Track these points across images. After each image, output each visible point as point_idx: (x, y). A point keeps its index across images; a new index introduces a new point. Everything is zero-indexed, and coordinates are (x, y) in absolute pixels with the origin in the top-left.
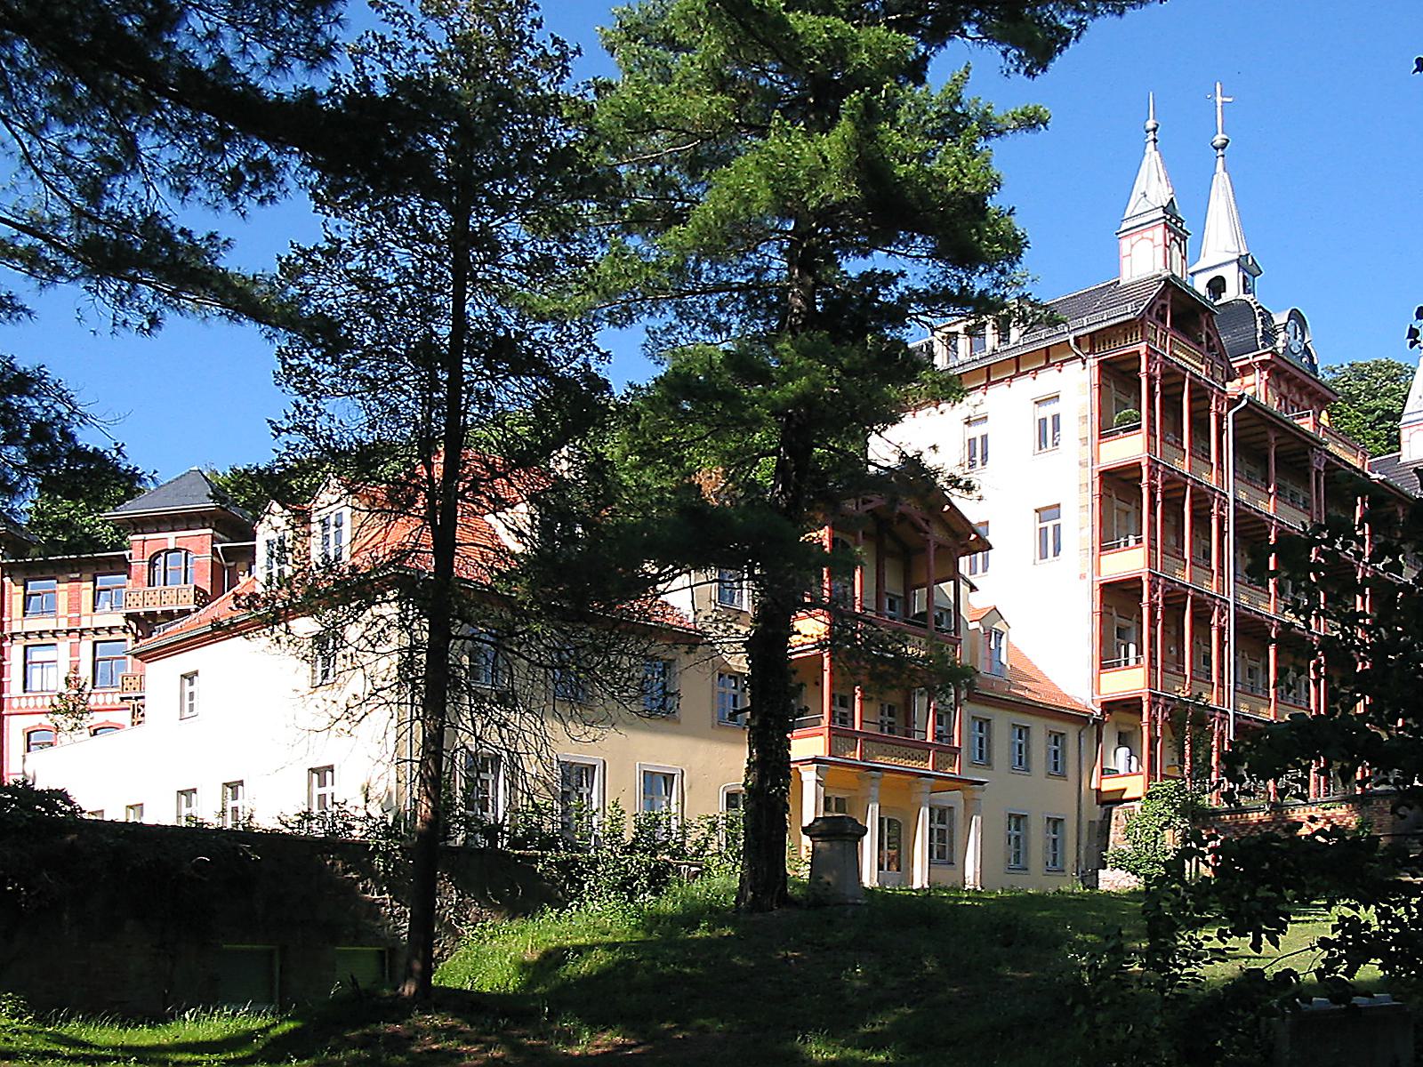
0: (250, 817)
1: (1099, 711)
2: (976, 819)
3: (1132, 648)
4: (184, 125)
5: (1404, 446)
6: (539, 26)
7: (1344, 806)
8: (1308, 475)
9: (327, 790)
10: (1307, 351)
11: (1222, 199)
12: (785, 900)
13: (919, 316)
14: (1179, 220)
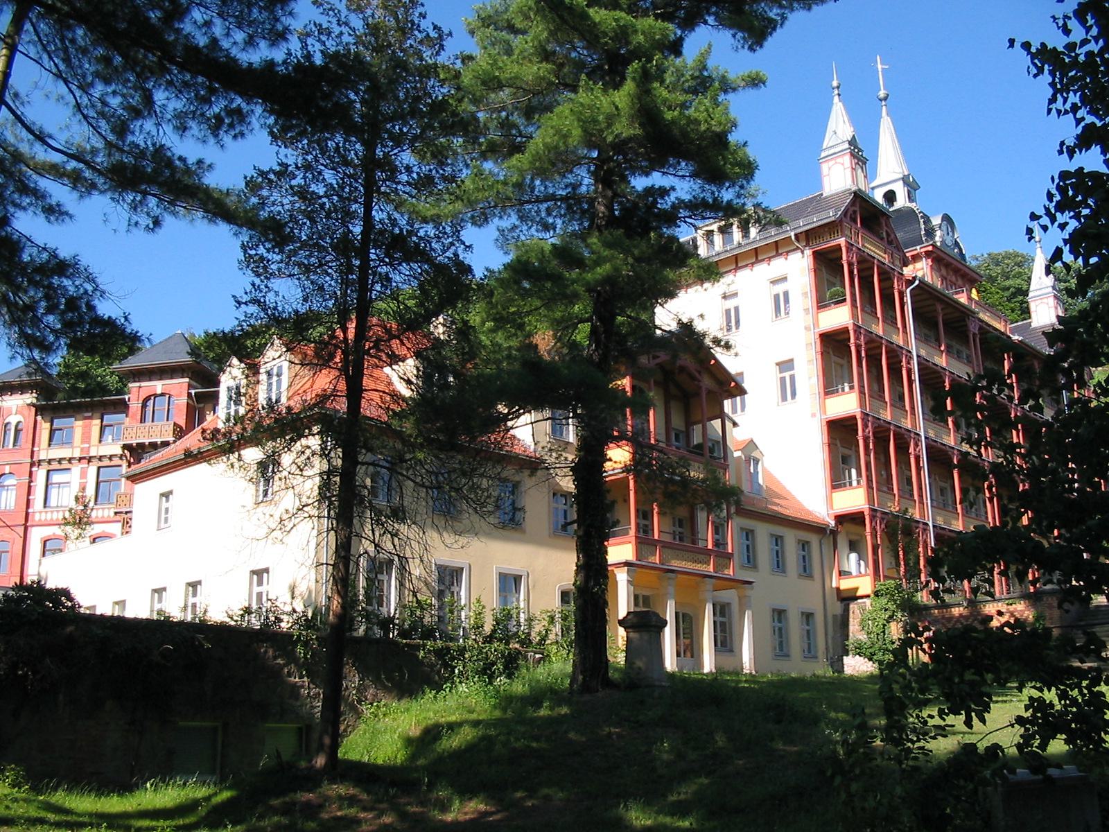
1: (833, 523)
2: (748, 615)
3: (854, 472)
5: (1033, 315)
6: (424, 18)
8: (968, 337)
10: (957, 244)
12: (609, 684)
14: (860, 150)
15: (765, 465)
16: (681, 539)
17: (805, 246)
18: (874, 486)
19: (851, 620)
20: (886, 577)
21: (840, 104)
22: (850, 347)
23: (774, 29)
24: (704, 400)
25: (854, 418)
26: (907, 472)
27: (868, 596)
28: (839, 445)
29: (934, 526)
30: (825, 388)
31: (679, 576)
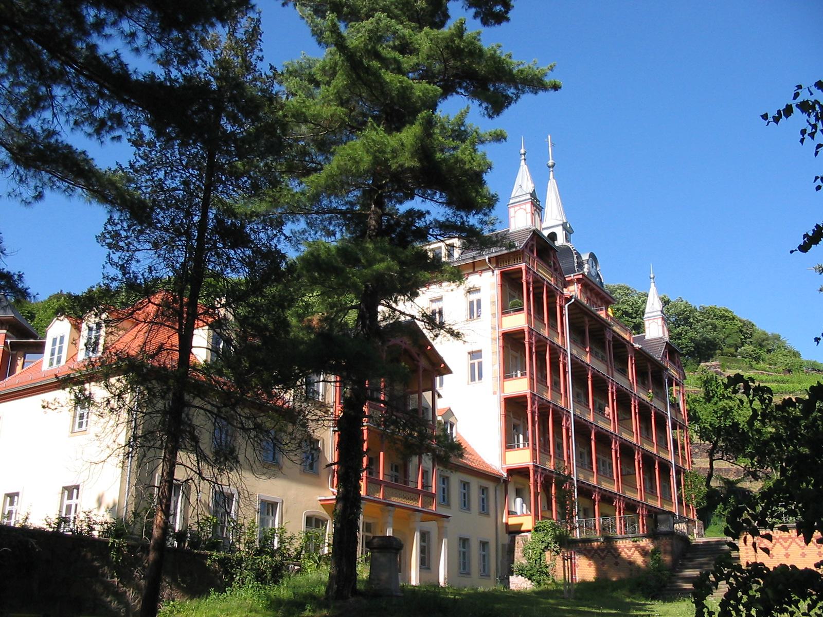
0: (27, 518)
1: (505, 475)
2: (444, 541)
3: (521, 437)
4: (80, 86)
5: (647, 330)
6: (261, 60)
7: (644, 540)
8: (604, 343)
9: (73, 502)
10: (598, 275)
11: (553, 192)
12: (356, 592)
13: (438, 237)
14: (538, 201)
15: (458, 431)
16: (396, 481)
17: (495, 268)
18: (537, 448)
19: (516, 548)
20: (543, 517)
21: (525, 166)
22: (525, 344)
23: (510, 104)
24: (421, 375)
25: (525, 396)
26: (560, 440)
27: (529, 531)
28: (512, 416)
29: (577, 481)
30: (504, 373)
31: (396, 509)
